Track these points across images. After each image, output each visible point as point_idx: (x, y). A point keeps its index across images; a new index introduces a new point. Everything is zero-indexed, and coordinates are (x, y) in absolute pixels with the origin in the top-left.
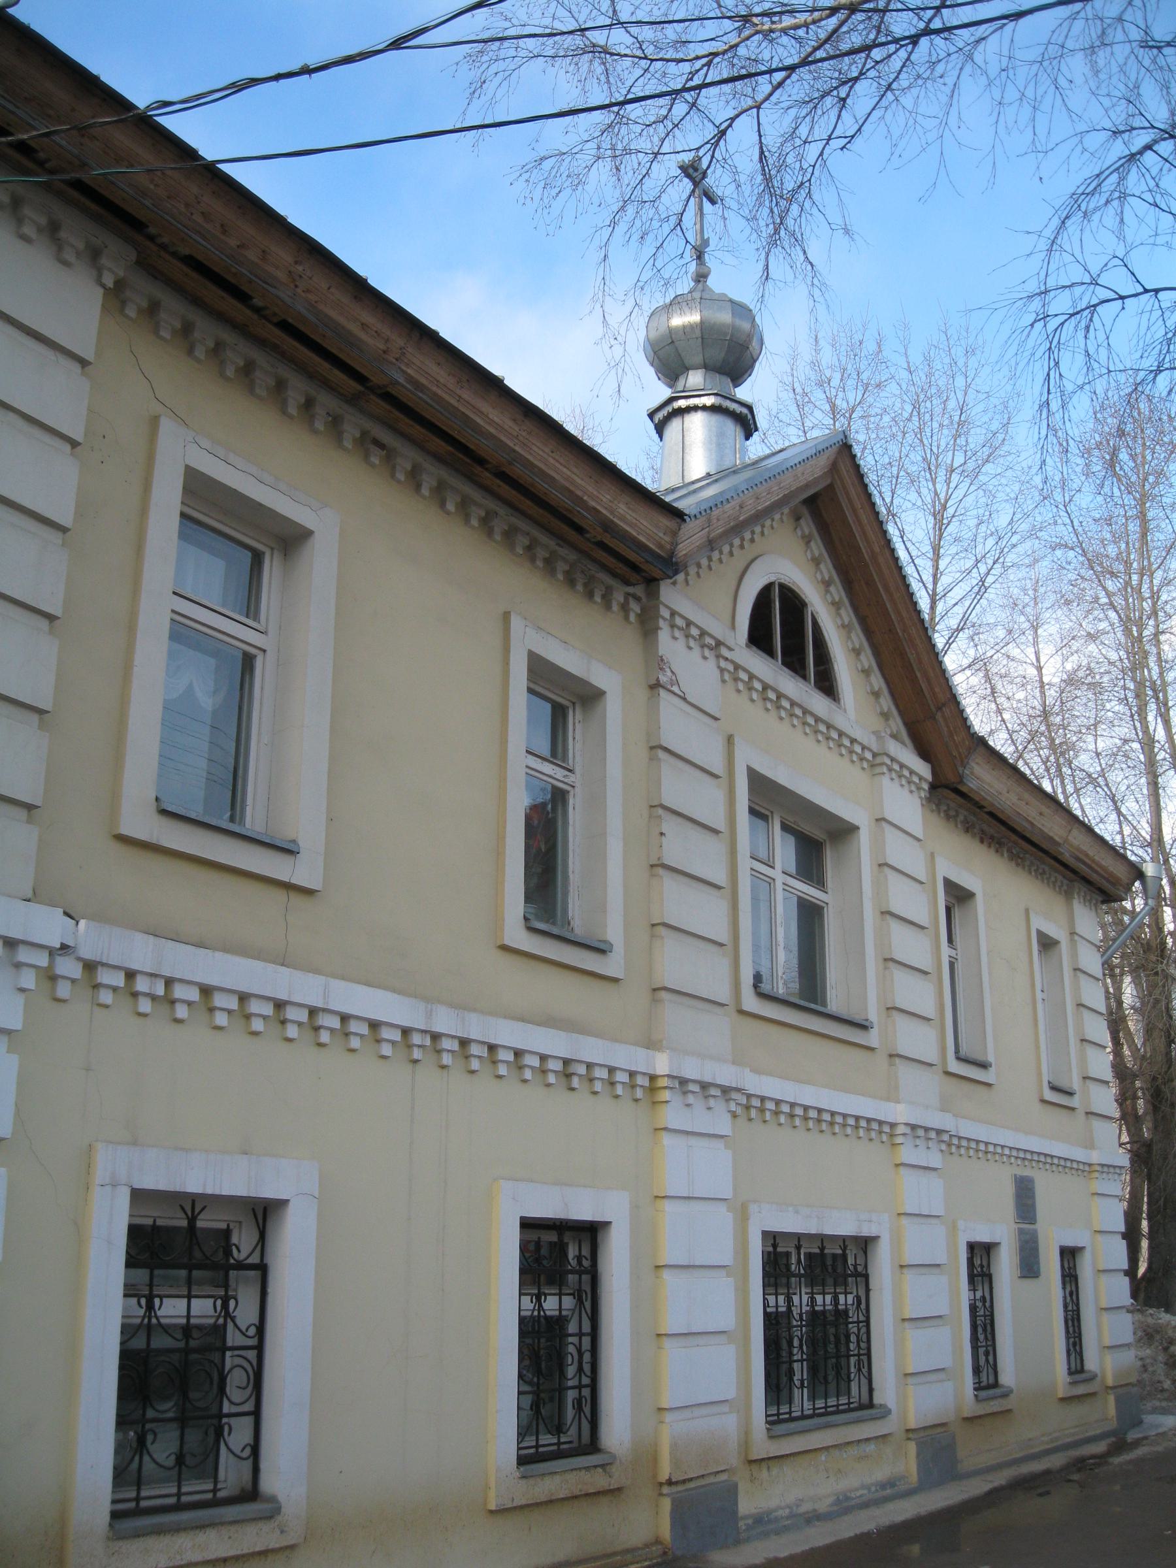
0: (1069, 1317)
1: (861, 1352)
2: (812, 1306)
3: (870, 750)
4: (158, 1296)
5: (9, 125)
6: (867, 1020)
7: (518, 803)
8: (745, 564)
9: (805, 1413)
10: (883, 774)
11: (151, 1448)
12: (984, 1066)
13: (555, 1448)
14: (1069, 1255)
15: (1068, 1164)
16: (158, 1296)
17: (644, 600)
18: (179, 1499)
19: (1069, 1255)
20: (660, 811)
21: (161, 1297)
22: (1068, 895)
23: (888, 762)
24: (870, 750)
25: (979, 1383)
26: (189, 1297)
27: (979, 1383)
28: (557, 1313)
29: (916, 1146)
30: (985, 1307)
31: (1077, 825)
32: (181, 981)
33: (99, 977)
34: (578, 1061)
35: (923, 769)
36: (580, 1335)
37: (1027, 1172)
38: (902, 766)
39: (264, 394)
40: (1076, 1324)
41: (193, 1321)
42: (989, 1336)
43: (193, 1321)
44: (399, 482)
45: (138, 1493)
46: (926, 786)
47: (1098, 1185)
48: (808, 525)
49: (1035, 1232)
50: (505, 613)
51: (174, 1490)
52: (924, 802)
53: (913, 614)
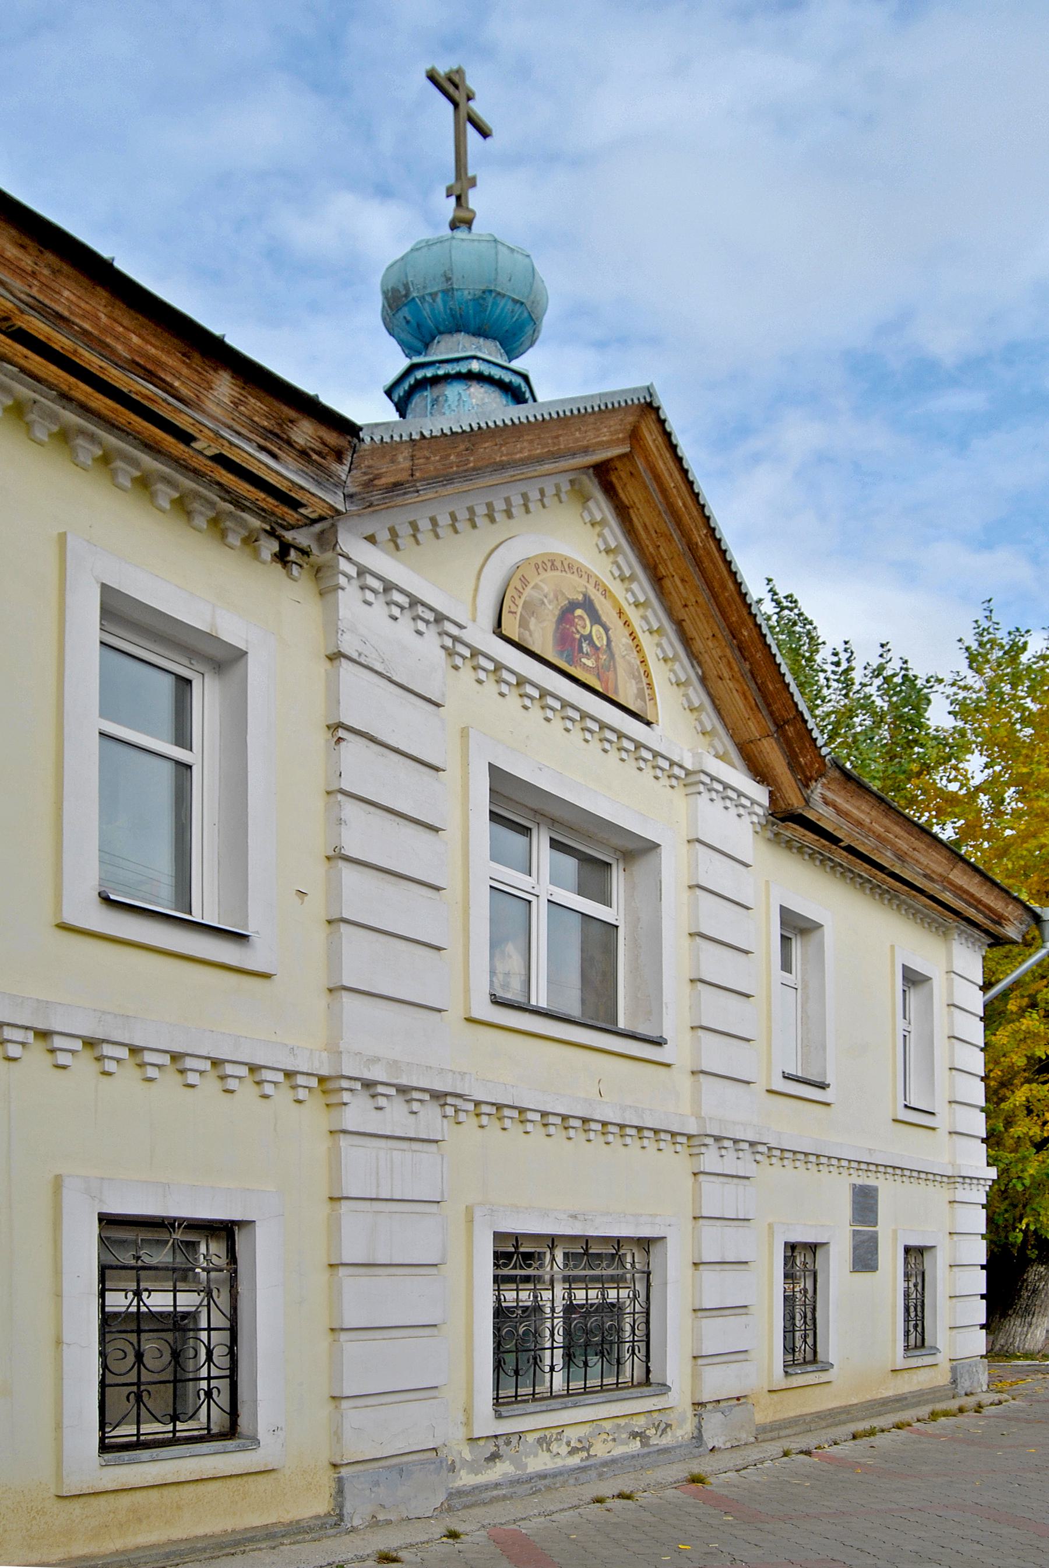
0: (912, 1304)
1: (555, 1345)
2: (604, 1299)
3: (681, 767)
4: (146, 1290)
5: (49, 339)
6: (661, 1037)
7: (900, 1034)
8: (498, 542)
9: (554, 1394)
10: (700, 793)
11: (575, 1360)
12: (822, 1086)
13: (135, 1439)
14: (915, 1253)
15: (923, 1176)
16: (146, 1290)
17: (315, 550)
18: (138, 1438)
19: (915, 1253)
20: (340, 797)
21: (150, 1291)
22: (944, 933)
23: (707, 780)
24: (681, 767)
25: (908, 1346)
26: (175, 1291)
27: (908, 1346)
28: (171, 1309)
29: (850, 1175)
30: (917, 1290)
31: (961, 864)
32: (9, 1025)
33: (5, 1033)
34: (743, 1141)
35: (760, 793)
36: (916, 1299)
37: (871, 1181)
38: (726, 786)
39: (128, 484)
40: (919, 1309)
41: (178, 1309)
42: (919, 1314)
43: (178, 1309)
44: (162, 510)
45: (138, 1429)
46: (760, 811)
47: (961, 1194)
48: (601, 508)
49: (876, 1233)
50: (463, 729)
51: (170, 1427)
52: (758, 829)
53: (747, 617)
